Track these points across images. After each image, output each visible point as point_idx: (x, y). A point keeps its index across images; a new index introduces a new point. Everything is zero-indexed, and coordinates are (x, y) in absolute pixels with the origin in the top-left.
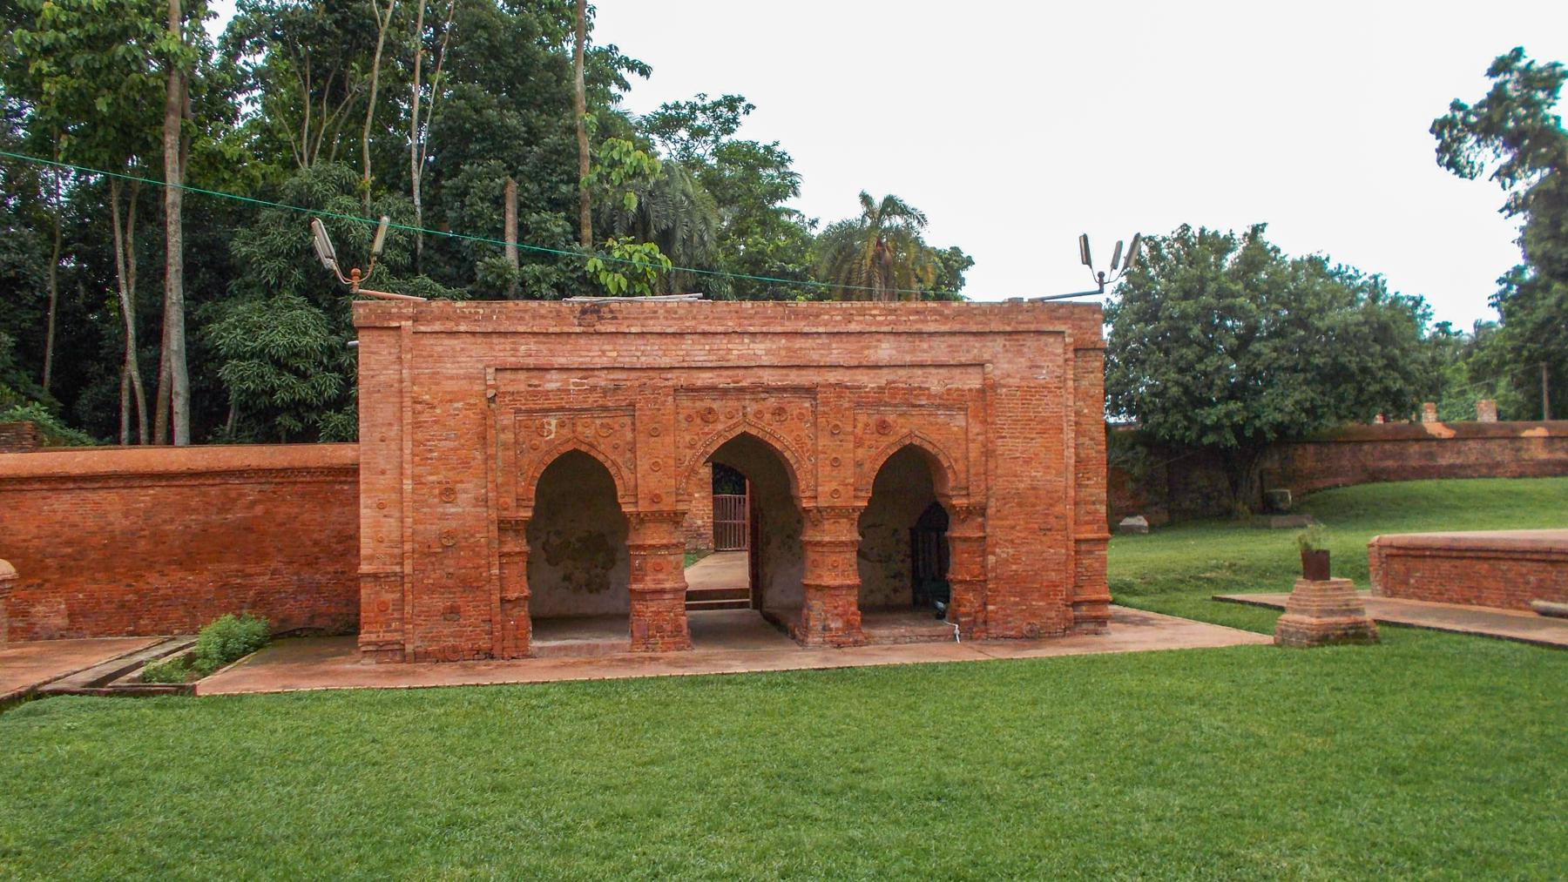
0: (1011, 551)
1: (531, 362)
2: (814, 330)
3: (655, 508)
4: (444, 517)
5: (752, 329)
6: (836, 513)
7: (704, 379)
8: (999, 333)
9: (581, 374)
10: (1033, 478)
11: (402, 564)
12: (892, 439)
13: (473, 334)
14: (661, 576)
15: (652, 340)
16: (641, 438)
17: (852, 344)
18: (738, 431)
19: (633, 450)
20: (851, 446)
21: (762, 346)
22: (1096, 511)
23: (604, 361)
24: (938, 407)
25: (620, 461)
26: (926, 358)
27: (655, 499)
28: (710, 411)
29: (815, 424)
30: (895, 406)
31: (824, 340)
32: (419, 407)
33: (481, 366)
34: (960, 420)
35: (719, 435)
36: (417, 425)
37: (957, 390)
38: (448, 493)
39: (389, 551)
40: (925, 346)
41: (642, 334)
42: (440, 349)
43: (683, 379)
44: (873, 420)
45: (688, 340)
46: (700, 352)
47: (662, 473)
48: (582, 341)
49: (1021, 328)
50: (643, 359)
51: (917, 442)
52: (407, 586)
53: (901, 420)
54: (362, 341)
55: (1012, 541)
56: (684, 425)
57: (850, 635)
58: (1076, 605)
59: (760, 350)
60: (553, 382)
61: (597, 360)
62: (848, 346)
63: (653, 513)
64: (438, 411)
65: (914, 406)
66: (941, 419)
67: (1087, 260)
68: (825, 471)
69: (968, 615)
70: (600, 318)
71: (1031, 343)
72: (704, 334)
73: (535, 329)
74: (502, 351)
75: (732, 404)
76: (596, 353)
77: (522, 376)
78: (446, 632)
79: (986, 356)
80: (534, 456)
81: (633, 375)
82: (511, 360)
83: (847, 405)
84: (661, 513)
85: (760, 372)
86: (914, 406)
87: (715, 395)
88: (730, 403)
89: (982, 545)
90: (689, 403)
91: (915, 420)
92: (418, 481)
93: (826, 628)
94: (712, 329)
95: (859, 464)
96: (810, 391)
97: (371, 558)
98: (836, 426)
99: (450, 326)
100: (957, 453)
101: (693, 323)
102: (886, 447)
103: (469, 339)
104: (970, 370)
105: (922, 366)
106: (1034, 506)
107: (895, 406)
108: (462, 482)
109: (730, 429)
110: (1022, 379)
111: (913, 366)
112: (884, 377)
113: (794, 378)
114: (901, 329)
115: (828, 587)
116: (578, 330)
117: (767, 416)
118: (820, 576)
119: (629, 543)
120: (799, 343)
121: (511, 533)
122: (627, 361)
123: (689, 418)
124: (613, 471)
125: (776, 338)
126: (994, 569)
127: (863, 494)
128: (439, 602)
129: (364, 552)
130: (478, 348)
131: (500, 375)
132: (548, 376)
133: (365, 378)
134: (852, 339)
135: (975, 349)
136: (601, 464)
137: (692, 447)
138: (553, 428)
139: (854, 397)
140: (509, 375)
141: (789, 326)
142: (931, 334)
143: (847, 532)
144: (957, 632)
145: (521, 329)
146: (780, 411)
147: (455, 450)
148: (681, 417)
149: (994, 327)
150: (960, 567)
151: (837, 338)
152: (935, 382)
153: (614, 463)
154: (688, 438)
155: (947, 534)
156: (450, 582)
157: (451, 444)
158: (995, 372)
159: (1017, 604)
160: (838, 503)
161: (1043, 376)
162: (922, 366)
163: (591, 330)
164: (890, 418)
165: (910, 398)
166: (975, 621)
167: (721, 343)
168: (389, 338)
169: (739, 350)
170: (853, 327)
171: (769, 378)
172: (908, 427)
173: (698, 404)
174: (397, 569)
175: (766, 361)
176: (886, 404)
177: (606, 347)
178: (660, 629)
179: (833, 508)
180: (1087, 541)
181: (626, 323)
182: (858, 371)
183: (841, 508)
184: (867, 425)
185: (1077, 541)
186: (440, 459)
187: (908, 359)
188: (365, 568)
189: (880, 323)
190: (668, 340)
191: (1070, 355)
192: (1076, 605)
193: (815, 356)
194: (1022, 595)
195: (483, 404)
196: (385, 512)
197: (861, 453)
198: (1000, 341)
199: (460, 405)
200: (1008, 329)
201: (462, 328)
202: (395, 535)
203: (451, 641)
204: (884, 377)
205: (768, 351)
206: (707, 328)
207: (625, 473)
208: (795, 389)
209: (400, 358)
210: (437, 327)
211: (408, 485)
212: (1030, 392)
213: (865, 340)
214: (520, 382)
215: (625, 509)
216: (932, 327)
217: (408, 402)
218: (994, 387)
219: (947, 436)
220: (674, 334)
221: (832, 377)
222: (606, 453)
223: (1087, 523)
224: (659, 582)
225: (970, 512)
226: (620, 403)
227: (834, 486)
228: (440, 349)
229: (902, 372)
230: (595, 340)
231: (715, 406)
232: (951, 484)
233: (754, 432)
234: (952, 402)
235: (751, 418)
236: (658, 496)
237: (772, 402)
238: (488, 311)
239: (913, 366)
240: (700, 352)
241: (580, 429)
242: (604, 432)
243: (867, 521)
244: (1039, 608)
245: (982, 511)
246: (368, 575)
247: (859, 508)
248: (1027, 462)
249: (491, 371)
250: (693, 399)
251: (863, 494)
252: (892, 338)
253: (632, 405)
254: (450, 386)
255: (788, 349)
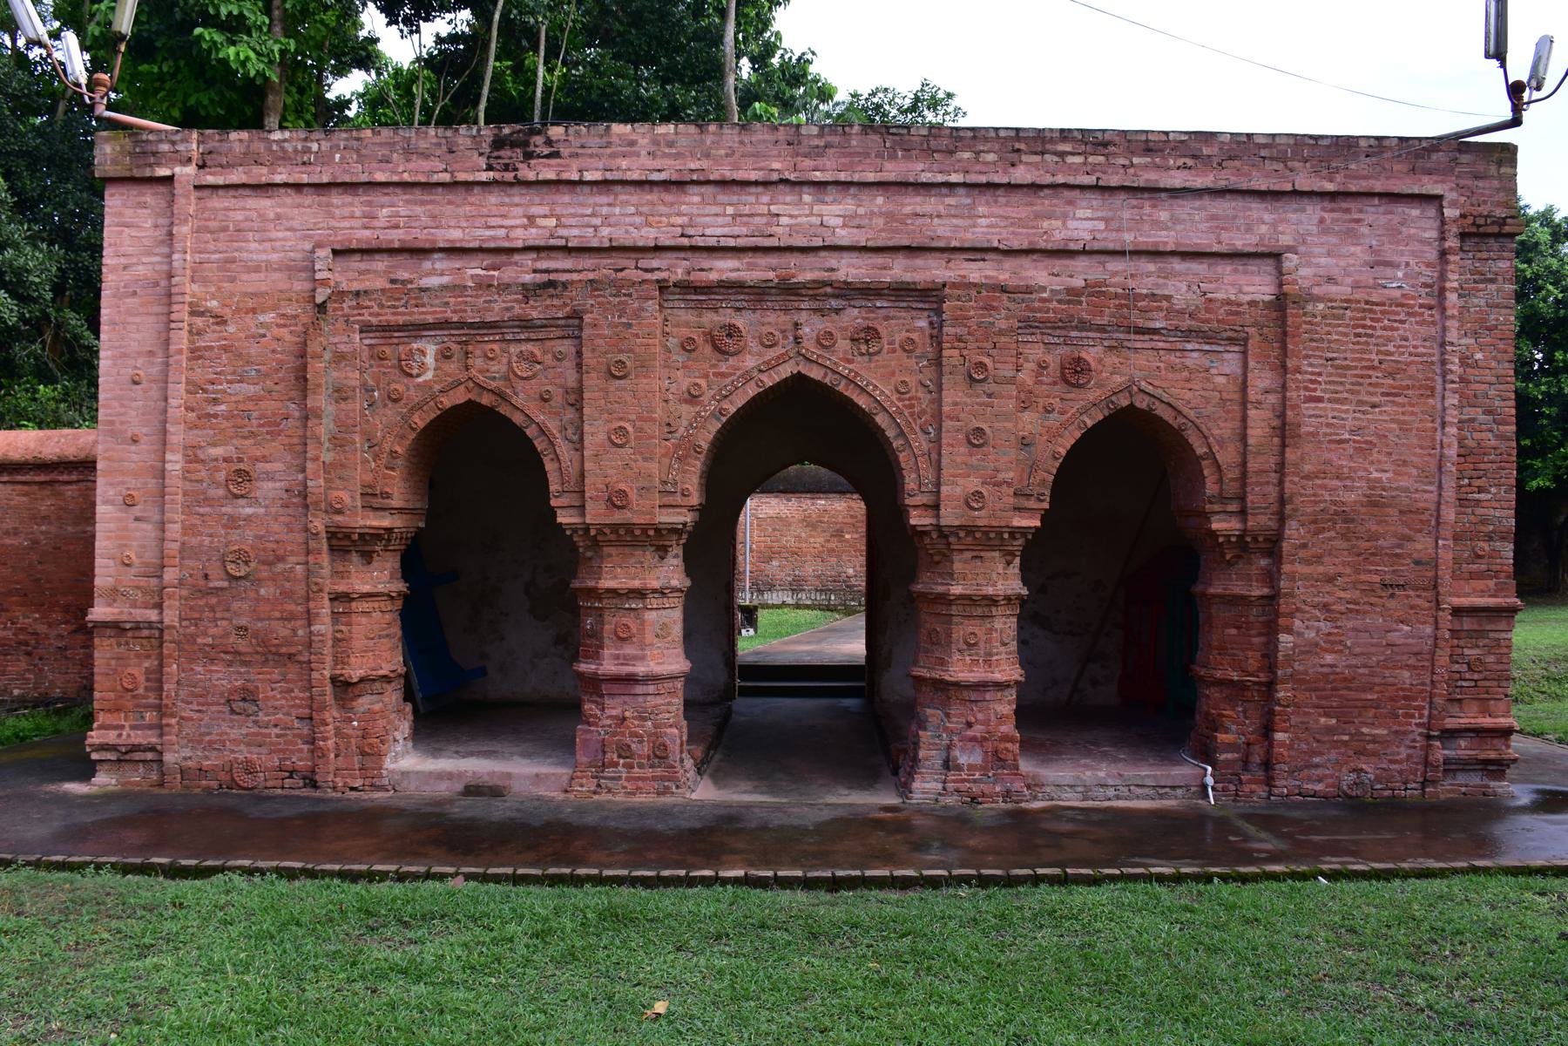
0: (1325, 627)
1: (396, 237)
2: (940, 178)
3: (618, 517)
4: (232, 522)
5: (818, 176)
6: (984, 539)
7: (724, 268)
8: (1311, 194)
9: (488, 260)
10: (1373, 484)
11: (159, 606)
12: (1092, 395)
13: (298, 187)
14: (629, 650)
15: (625, 195)
16: (592, 381)
17: (1018, 208)
18: (786, 371)
19: (578, 405)
20: (1011, 405)
21: (837, 209)
22: (1495, 554)
23: (533, 236)
24: (1189, 334)
25: (552, 425)
26: (1166, 239)
27: (616, 500)
28: (732, 331)
29: (937, 362)
30: (1101, 329)
31: (961, 199)
32: (199, 321)
33: (308, 246)
34: (1230, 362)
35: (747, 377)
36: (196, 354)
37: (1229, 302)
38: (241, 479)
39: (143, 582)
40: (1164, 215)
41: (605, 185)
42: (239, 216)
43: (677, 269)
44: (1053, 360)
45: (694, 196)
46: (714, 219)
47: (627, 449)
48: (493, 198)
49: (1353, 187)
50: (605, 231)
51: (1142, 403)
52: (168, 648)
53: (1112, 359)
54: (115, 203)
55: (1326, 607)
56: (679, 358)
57: (997, 779)
58: (1450, 735)
59: (834, 217)
60: (435, 274)
61: (519, 233)
62: (1009, 211)
63: (615, 527)
64: (231, 329)
65: (1140, 331)
66: (1194, 359)
67: (1498, 52)
68: (955, 454)
69: (1231, 747)
70: (529, 156)
71: (1374, 214)
72: (724, 184)
73: (406, 177)
74: (349, 219)
75: (774, 319)
76: (513, 219)
77: (380, 264)
78: (235, 733)
79: (1286, 240)
80: (391, 414)
81: (587, 262)
82: (363, 236)
83: (1003, 324)
84: (629, 527)
85: (832, 260)
86: (1140, 331)
87: (741, 300)
88: (771, 317)
89: (1271, 613)
90: (690, 317)
91: (1141, 360)
92: (193, 456)
93: (948, 764)
94: (740, 175)
95: (1025, 443)
96: (929, 296)
97: (114, 594)
98: (982, 365)
99: (262, 174)
100: (1223, 429)
101: (704, 164)
102: (1077, 414)
103: (291, 198)
104: (1253, 266)
105: (1155, 254)
106: (1372, 537)
107: (1101, 329)
108: (265, 459)
109: (770, 367)
110: (1356, 286)
111: (1137, 253)
112: (1080, 273)
113: (899, 270)
114: (1114, 180)
115: (957, 684)
116: (484, 176)
117: (843, 345)
118: (942, 663)
119: (576, 584)
120: (913, 203)
121: (355, 557)
122: (574, 234)
123: (688, 346)
124: (540, 445)
125: (865, 195)
126: (1290, 660)
127: (1032, 504)
128: (223, 678)
129: (102, 580)
130: (303, 214)
131: (341, 263)
132: (427, 265)
133: (114, 269)
134: (1017, 197)
135: (1259, 225)
136: (518, 432)
137: (692, 398)
138: (430, 360)
139: (1018, 309)
140: (355, 263)
141: (892, 171)
142: (1175, 193)
143: (1005, 579)
144: (1210, 780)
145: (380, 177)
146: (867, 336)
147: (256, 399)
148: (673, 342)
149: (1304, 182)
150: (1225, 659)
151: (988, 196)
152: (1181, 286)
153: (542, 431)
154: (685, 384)
155: (1199, 588)
156: (242, 645)
157: (251, 389)
158: (1302, 273)
159: (1329, 730)
160: (982, 518)
161: (1396, 283)
162: (1155, 254)
163: (509, 176)
164: (1091, 354)
165: (1129, 321)
166: (1246, 763)
167: (758, 202)
168: (151, 197)
169: (795, 217)
170: (1021, 175)
171: (850, 269)
172: (1125, 373)
173: (709, 318)
174: (153, 615)
175: (844, 236)
176: (1083, 326)
177: (535, 210)
178: (625, 751)
179: (970, 530)
180: (1473, 611)
181: (575, 164)
182: (1025, 261)
183: (986, 531)
184: (1042, 366)
185: (1457, 612)
186: (229, 416)
187: (1129, 239)
188: (100, 612)
189: (1074, 169)
190: (652, 196)
191: (1453, 242)
192: (1450, 735)
193: (945, 230)
194: (1344, 716)
195: (304, 313)
196: (137, 511)
197: (1030, 422)
198: (1312, 213)
199: (268, 317)
200: (1330, 187)
201: (278, 179)
202: (151, 556)
203: (243, 753)
204: (1080, 273)
205: (849, 220)
206: (729, 175)
207: (564, 449)
208: (900, 292)
209: (170, 234)
210: (237, 176)
211: (175, 463)
212: (1367, 312)
213: (1044, 202)
214: (375, 275)
215: (563, 518)
216: (1177, 180)
217: (182, 313)
218: (1285, 294)
219: (1194, 388)
220: (666, 184)
221: (976, 272)
222: (531, 407)
223: (1473, 576)
224: (627, 660)
225: (1243, 545)
226: (558, 304)
227: (973, 483)
228: (239, 216)
229: (1115, 265)
230: (517, 196)
231: (740, 322)
232: (1211, 488)
233: (815, 374)
234: (1211, 329)
235: (809, 345)
236: (623, 494)
237: (853, 316)
238: (325, 145)
239: (1137, 253)
240: (714, 219)
241: (479, 362)
242: (522, 369)
243: (1036, 554)
244: (1374, 740)
245: (1272, 545)
246: (105, 625)
247: (1023, 531)
248: (1364, 450)
249: (324, 253)
250: (699, 307)
251: (1032, 504)
252: (1095, 199)
253: (576, 315)
254: (253, 282)
255: (889, 216)
